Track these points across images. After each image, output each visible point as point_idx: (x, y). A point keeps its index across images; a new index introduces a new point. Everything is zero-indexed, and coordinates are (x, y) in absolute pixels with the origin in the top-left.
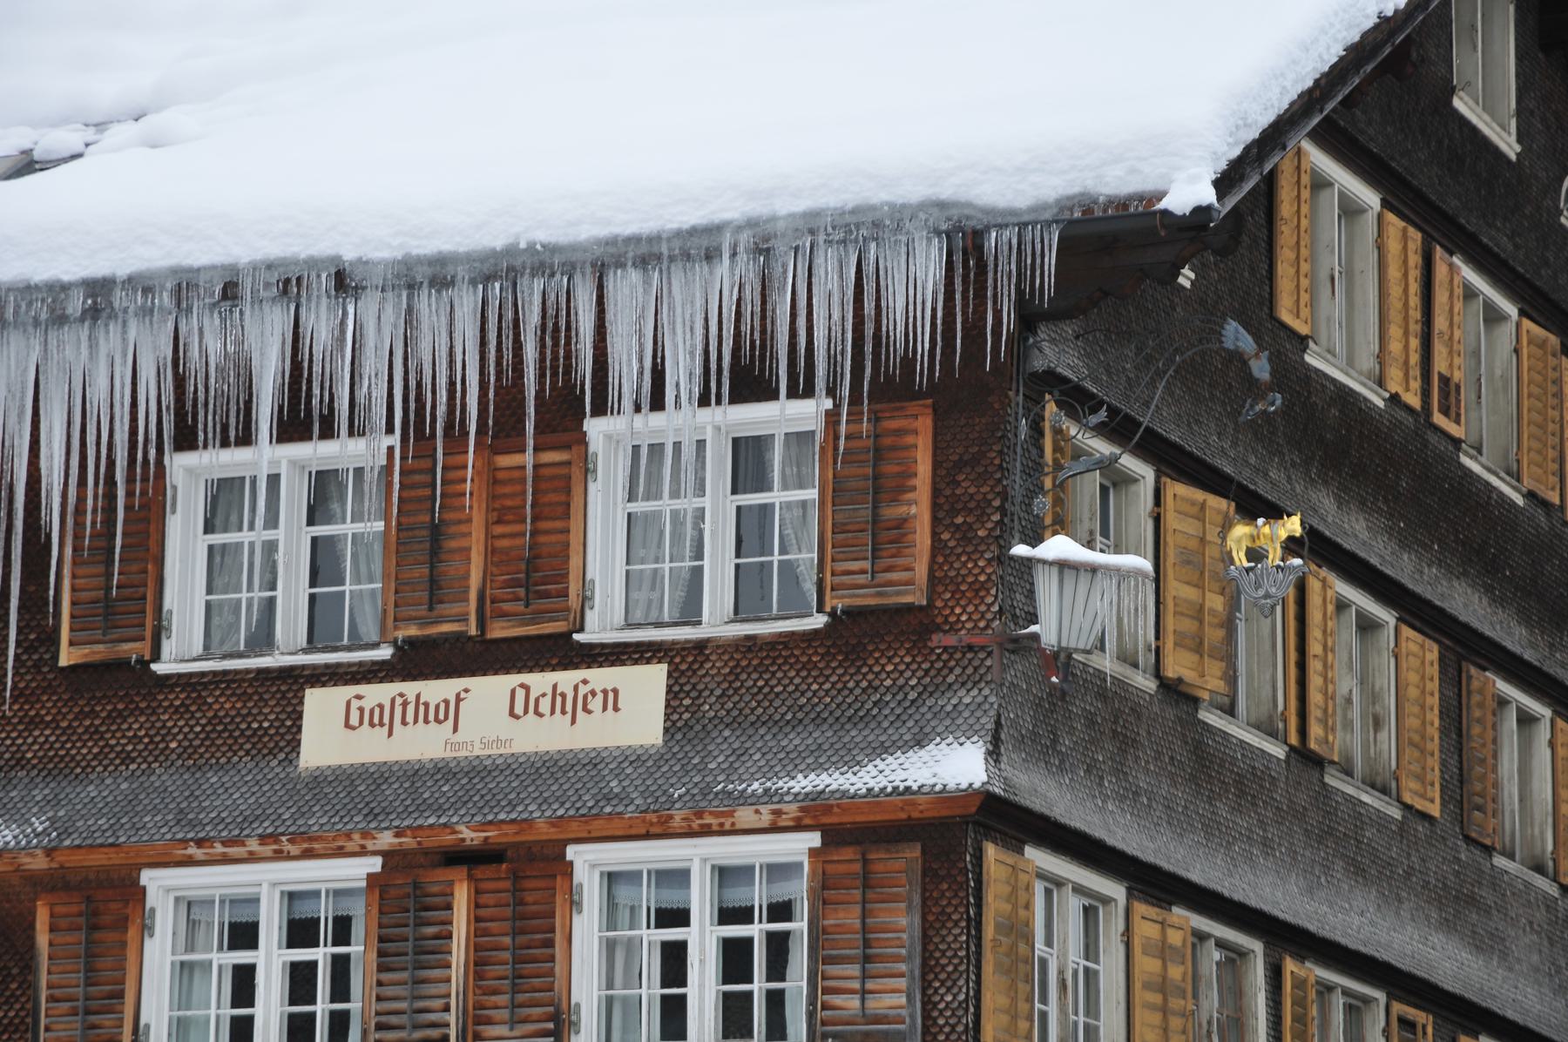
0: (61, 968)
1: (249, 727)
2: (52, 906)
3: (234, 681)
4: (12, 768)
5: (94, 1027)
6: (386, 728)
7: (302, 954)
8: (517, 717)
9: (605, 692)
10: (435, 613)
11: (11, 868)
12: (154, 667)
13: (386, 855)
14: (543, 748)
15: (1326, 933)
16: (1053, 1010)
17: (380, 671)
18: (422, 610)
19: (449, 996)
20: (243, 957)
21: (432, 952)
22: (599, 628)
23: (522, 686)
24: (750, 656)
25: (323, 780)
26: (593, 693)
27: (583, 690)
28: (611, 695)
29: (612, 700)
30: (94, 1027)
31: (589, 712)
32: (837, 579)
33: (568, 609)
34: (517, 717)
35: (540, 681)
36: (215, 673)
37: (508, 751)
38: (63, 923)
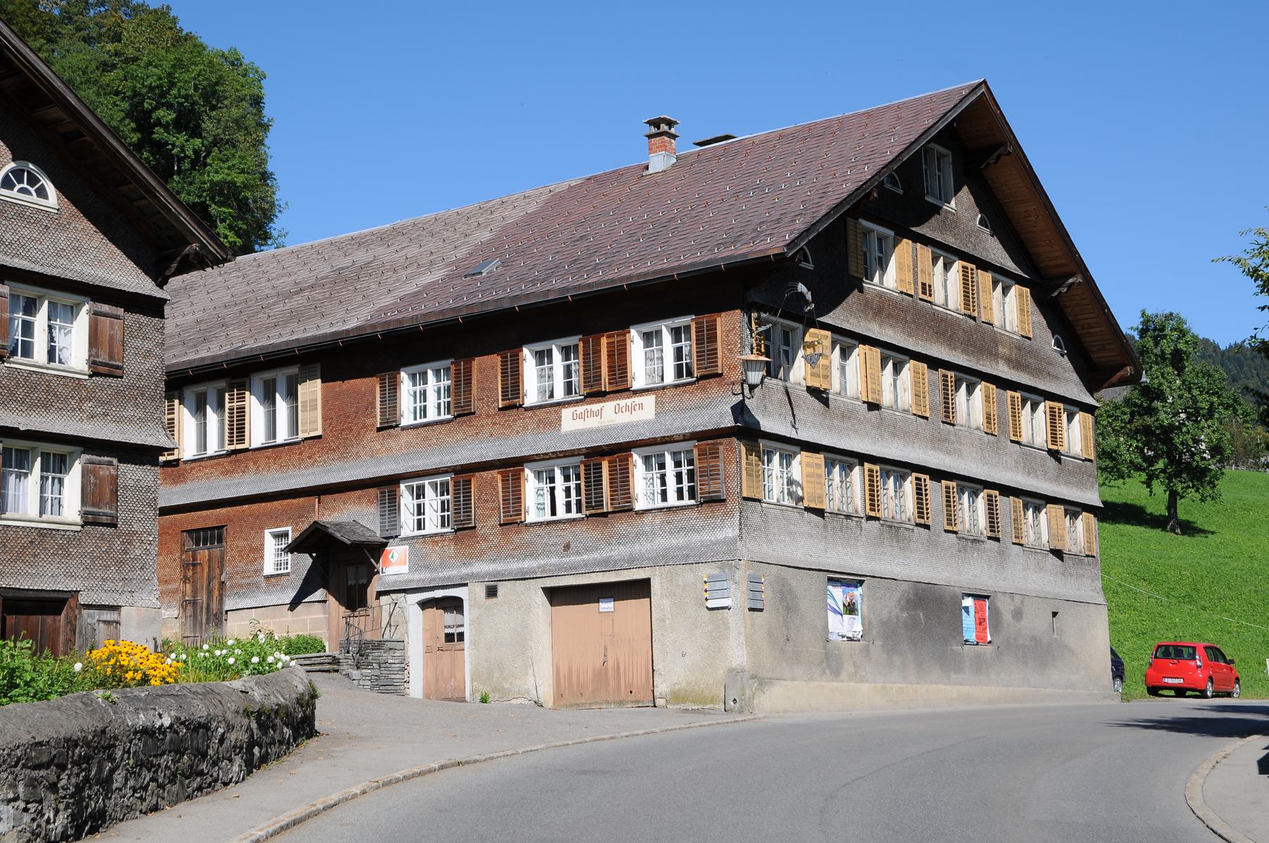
7: (567, 484)
22: (637, 385)
35: (622, 402)
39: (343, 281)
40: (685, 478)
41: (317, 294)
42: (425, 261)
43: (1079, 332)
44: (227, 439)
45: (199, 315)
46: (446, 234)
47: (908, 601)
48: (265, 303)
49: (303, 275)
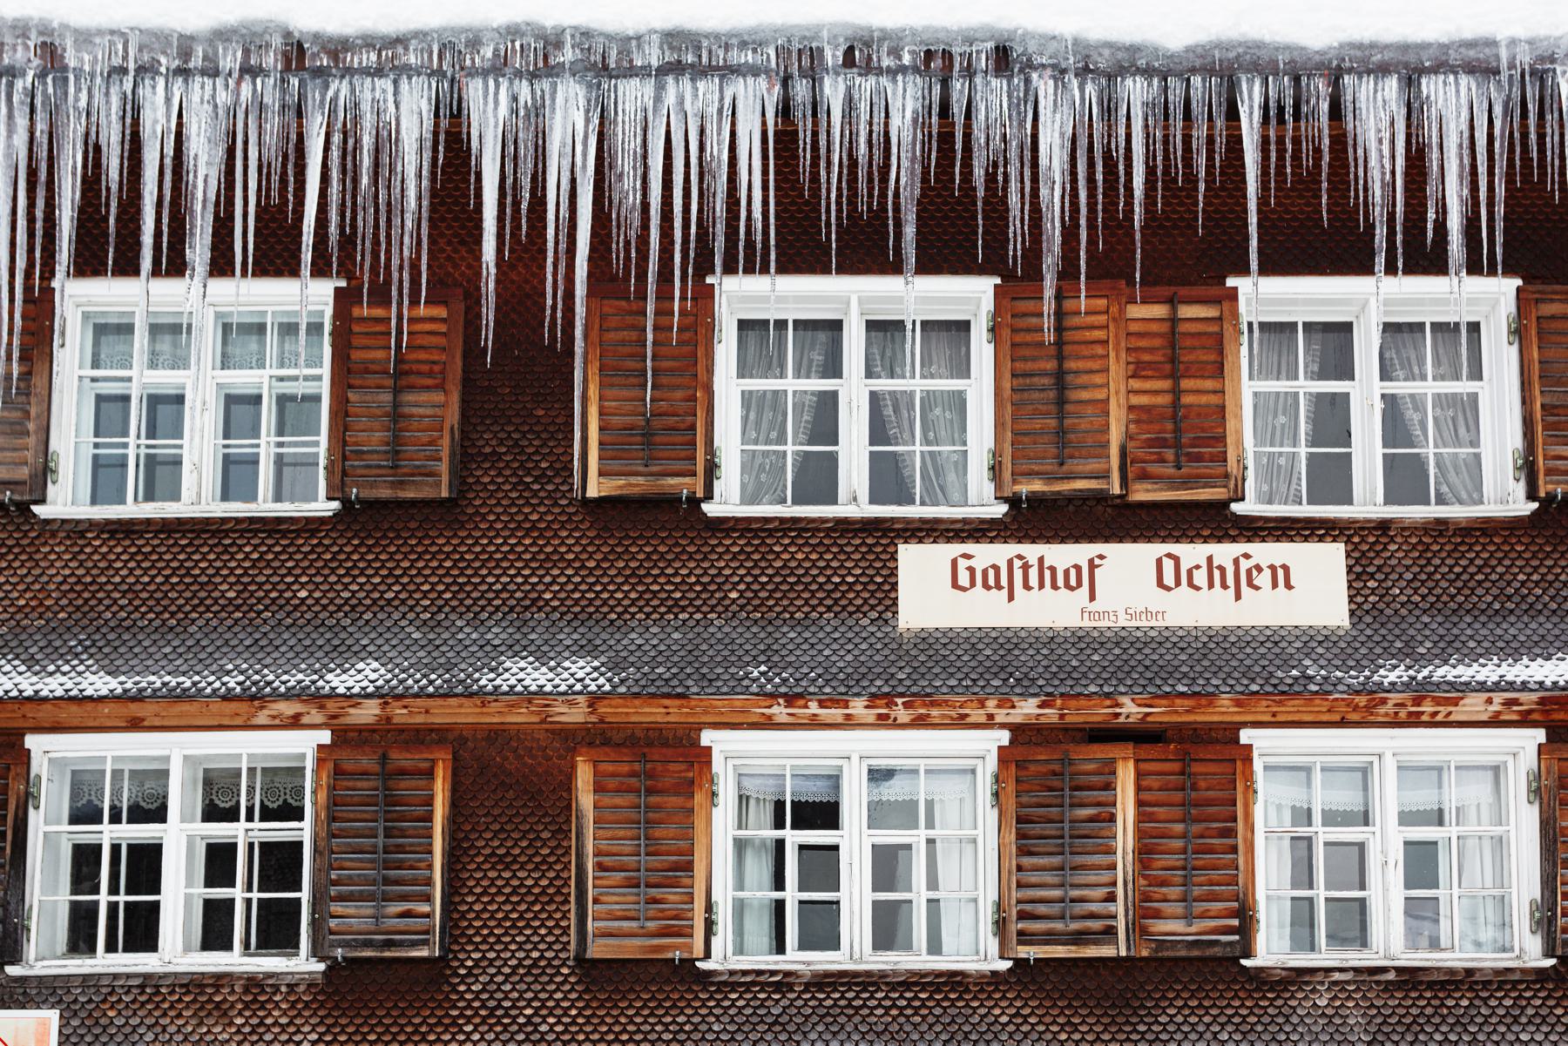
0: (609, 834)
1: (829, 580)
2: (595, 763)
3: (807, 530)
4: (526, 608)
5: (655, 901)
6: (1005, 591)
8: (1169, 589)
9: (1273, 568)
10: (1065, 468)
11: (535, 719)
12: (705, 507)
13: (1015, 729)
14: (1204, 622)
17: (990, 530)
18: (1049, 465)
19: (1114, 884)
23: (1169, 555)
24: (1441, 540)
25: (928, 641)
26: (1259, 568)
27: (1245, 565)
28: (1280, 572)
30: (655, 901)
31: (1257, 588)
32: (1551, 463)
33: (1227, 476)
34: (1169, 589)
35: (1192, 553)
36: (782, 520)
37: (1161, 623)
38: (612, 783)
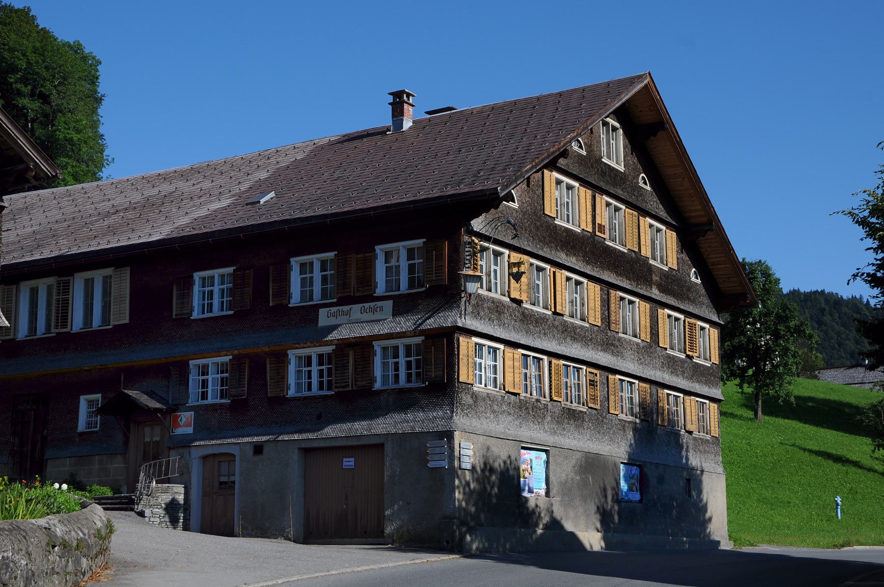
15: (564, 353)
16: (483, 373)
20: (309, 369)
21: (345, 367)
29: (381, 308)
35: (367, 305)
39: (149, 207)
40: (414, 365)
41: (130, 215)
42: (216, 192)
43: (711, 267)
44: (53, 324)
45: (34, 228)
46: (233, 174)
47: (581, 466)
48: (88, 220)
49: (119, 201)
